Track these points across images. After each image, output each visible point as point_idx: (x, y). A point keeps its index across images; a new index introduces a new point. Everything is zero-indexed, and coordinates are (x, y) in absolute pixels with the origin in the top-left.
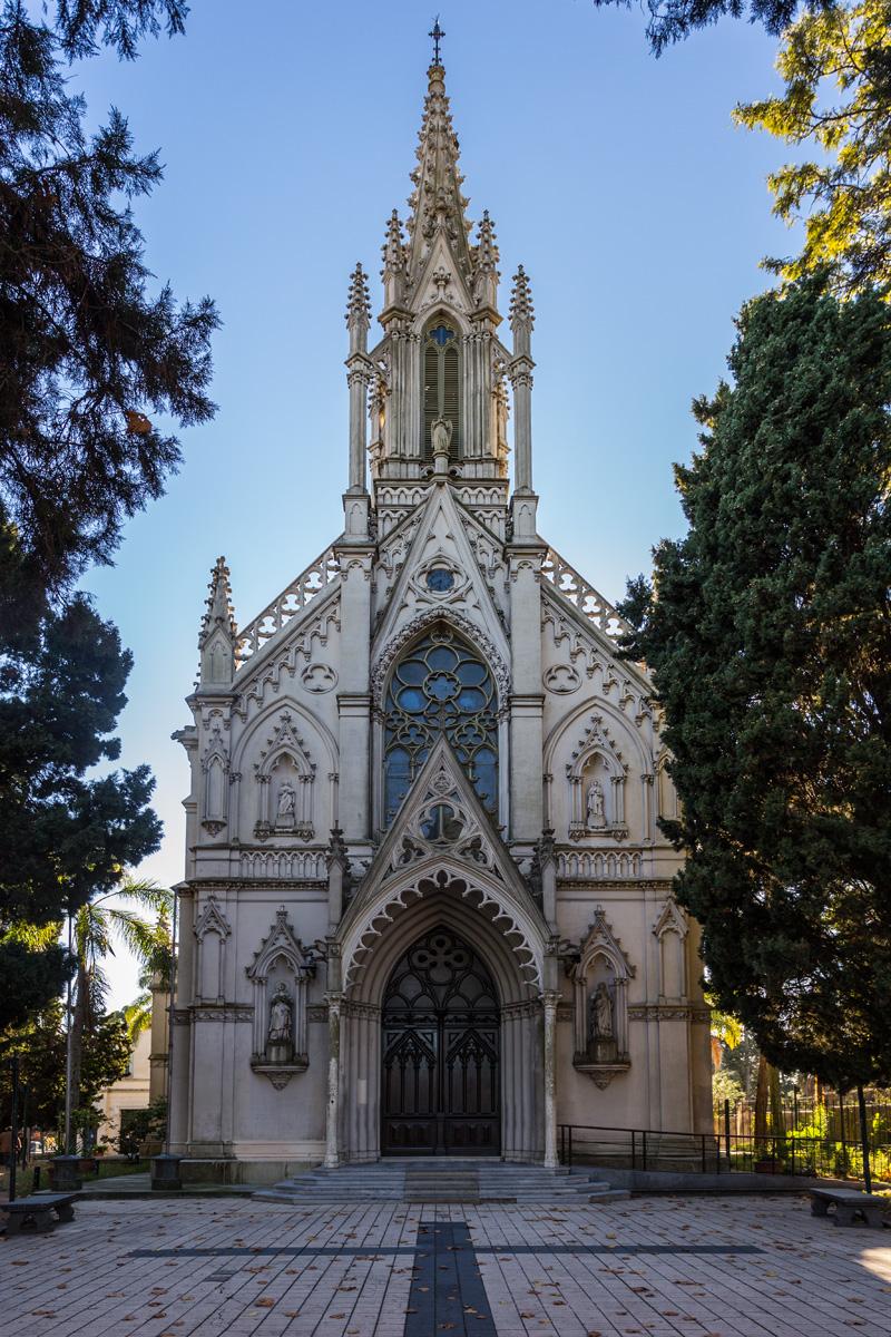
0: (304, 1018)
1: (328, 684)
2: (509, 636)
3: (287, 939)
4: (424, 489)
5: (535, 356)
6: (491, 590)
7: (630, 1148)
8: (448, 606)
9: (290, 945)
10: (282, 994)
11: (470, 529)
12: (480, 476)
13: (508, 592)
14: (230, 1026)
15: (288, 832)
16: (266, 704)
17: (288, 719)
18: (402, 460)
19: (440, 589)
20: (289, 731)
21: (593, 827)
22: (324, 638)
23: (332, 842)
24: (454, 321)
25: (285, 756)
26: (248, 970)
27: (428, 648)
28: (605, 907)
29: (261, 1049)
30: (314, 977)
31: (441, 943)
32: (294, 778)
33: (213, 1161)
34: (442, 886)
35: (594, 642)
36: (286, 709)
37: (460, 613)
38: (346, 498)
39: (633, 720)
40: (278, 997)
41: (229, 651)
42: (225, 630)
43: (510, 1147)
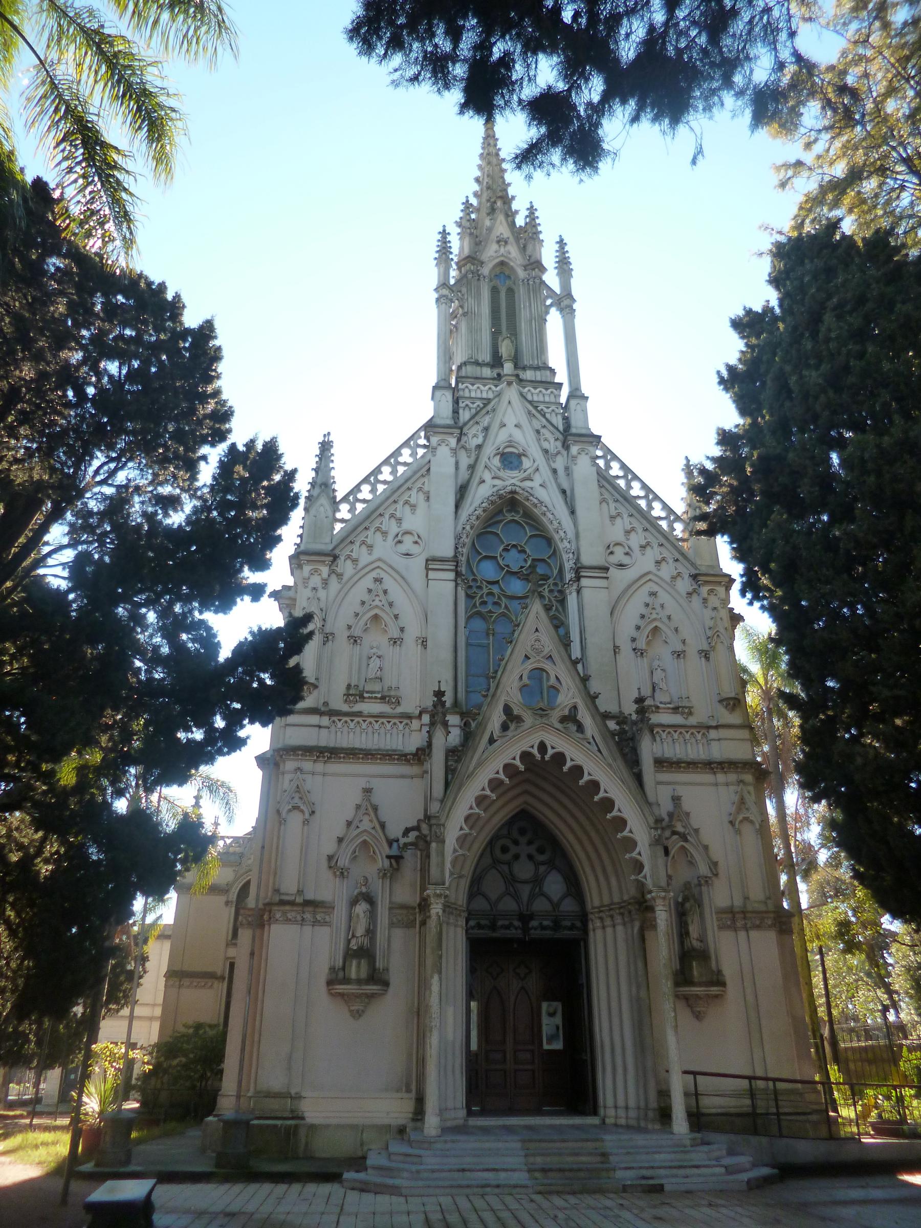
0: (386, 921)
1: (415, 549)
2: (573, 512)
3: (371, 821)
4: (496, 386)
5: (574, 293)
6: (555, 471)
7: (748, 1102)
8: (518, 483)
9: (374, 828)
10: (364, 890)
11: (534, 421)
12: (539, 379)
13: (568, 475)
14: (308, 929)
15: (376, 698)
16: (361, 565)
17: (378, 580)
18: (477, 363)
19: (511, 469)
20: (381, 593)
21: (661, 703)
22: (413, 507)
23: (435, 706)
24: (512, 269)
25: (376, 617)
26: (330, 858)
27: (501, 521)
28: (681, 791)
29: (340, 963)
30: (397, 870)
31: (522, 832)
32: (384, 640)
33: (279, 1122)
34: (543, 758)
35: (644, 522)
36: (378, 571)
37: (529, 490)
38: (435, 388)
39: (685, 595)
40: (361, 894)
41: (330, 514)
42: (328, 496)
43: (610, 1102)
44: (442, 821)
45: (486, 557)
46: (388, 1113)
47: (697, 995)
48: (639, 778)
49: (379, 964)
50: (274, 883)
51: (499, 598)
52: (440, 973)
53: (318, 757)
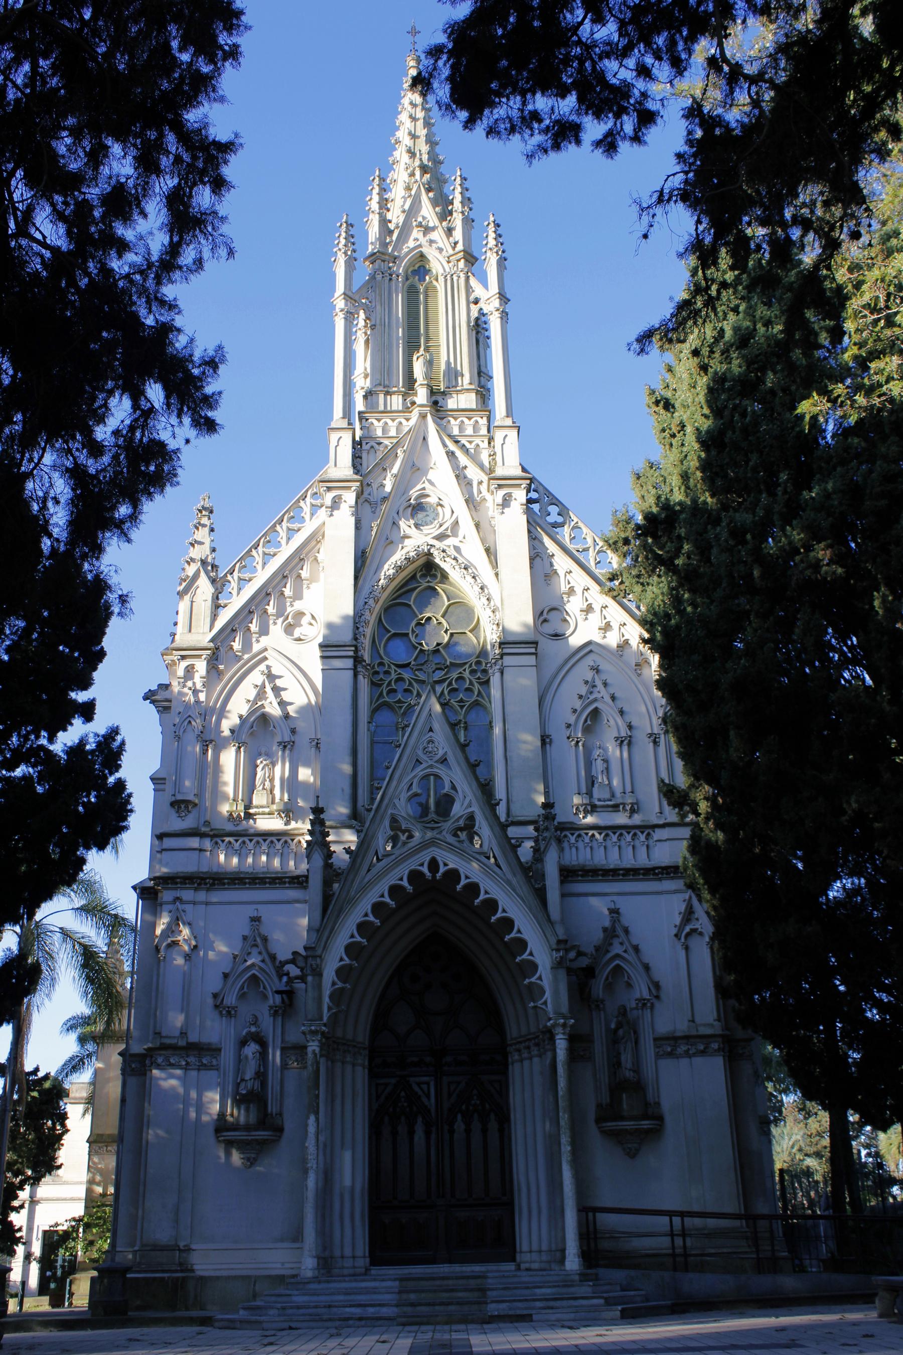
10: (253, 1029)
21: (599, 800)
27: (415, 588)
34: (434, 876)
40: (249, 1033)
43: (525, 1248)
44: (319, 952)
45: (395, 635)
46: (283, 1264)
47: (626, 1130)
48: (541, 894)
49: (272, 1108)
50: (155, 1027)
51: (410, 684)
52: (317, 1113)
53: (199, 884)
